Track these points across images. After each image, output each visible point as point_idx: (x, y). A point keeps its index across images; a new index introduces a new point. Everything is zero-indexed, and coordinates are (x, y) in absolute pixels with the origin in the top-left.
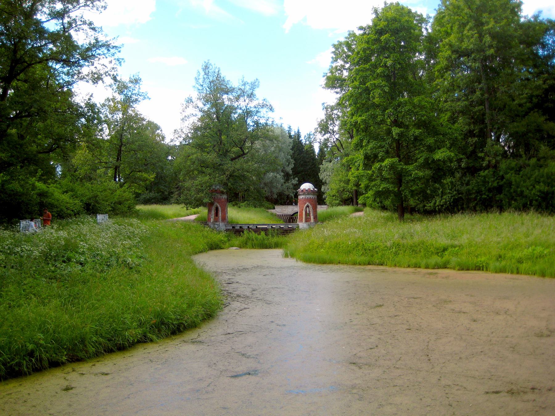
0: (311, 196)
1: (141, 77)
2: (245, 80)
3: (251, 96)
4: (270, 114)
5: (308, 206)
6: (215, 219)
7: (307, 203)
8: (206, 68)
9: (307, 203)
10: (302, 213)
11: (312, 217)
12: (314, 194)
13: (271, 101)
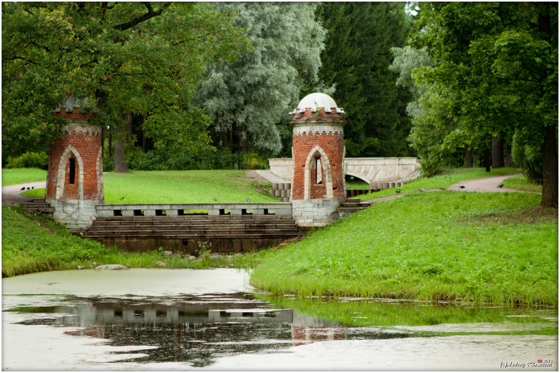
0: (328, 129)
5: (317, 157)
9: (317, 148)
12: (334, 123)
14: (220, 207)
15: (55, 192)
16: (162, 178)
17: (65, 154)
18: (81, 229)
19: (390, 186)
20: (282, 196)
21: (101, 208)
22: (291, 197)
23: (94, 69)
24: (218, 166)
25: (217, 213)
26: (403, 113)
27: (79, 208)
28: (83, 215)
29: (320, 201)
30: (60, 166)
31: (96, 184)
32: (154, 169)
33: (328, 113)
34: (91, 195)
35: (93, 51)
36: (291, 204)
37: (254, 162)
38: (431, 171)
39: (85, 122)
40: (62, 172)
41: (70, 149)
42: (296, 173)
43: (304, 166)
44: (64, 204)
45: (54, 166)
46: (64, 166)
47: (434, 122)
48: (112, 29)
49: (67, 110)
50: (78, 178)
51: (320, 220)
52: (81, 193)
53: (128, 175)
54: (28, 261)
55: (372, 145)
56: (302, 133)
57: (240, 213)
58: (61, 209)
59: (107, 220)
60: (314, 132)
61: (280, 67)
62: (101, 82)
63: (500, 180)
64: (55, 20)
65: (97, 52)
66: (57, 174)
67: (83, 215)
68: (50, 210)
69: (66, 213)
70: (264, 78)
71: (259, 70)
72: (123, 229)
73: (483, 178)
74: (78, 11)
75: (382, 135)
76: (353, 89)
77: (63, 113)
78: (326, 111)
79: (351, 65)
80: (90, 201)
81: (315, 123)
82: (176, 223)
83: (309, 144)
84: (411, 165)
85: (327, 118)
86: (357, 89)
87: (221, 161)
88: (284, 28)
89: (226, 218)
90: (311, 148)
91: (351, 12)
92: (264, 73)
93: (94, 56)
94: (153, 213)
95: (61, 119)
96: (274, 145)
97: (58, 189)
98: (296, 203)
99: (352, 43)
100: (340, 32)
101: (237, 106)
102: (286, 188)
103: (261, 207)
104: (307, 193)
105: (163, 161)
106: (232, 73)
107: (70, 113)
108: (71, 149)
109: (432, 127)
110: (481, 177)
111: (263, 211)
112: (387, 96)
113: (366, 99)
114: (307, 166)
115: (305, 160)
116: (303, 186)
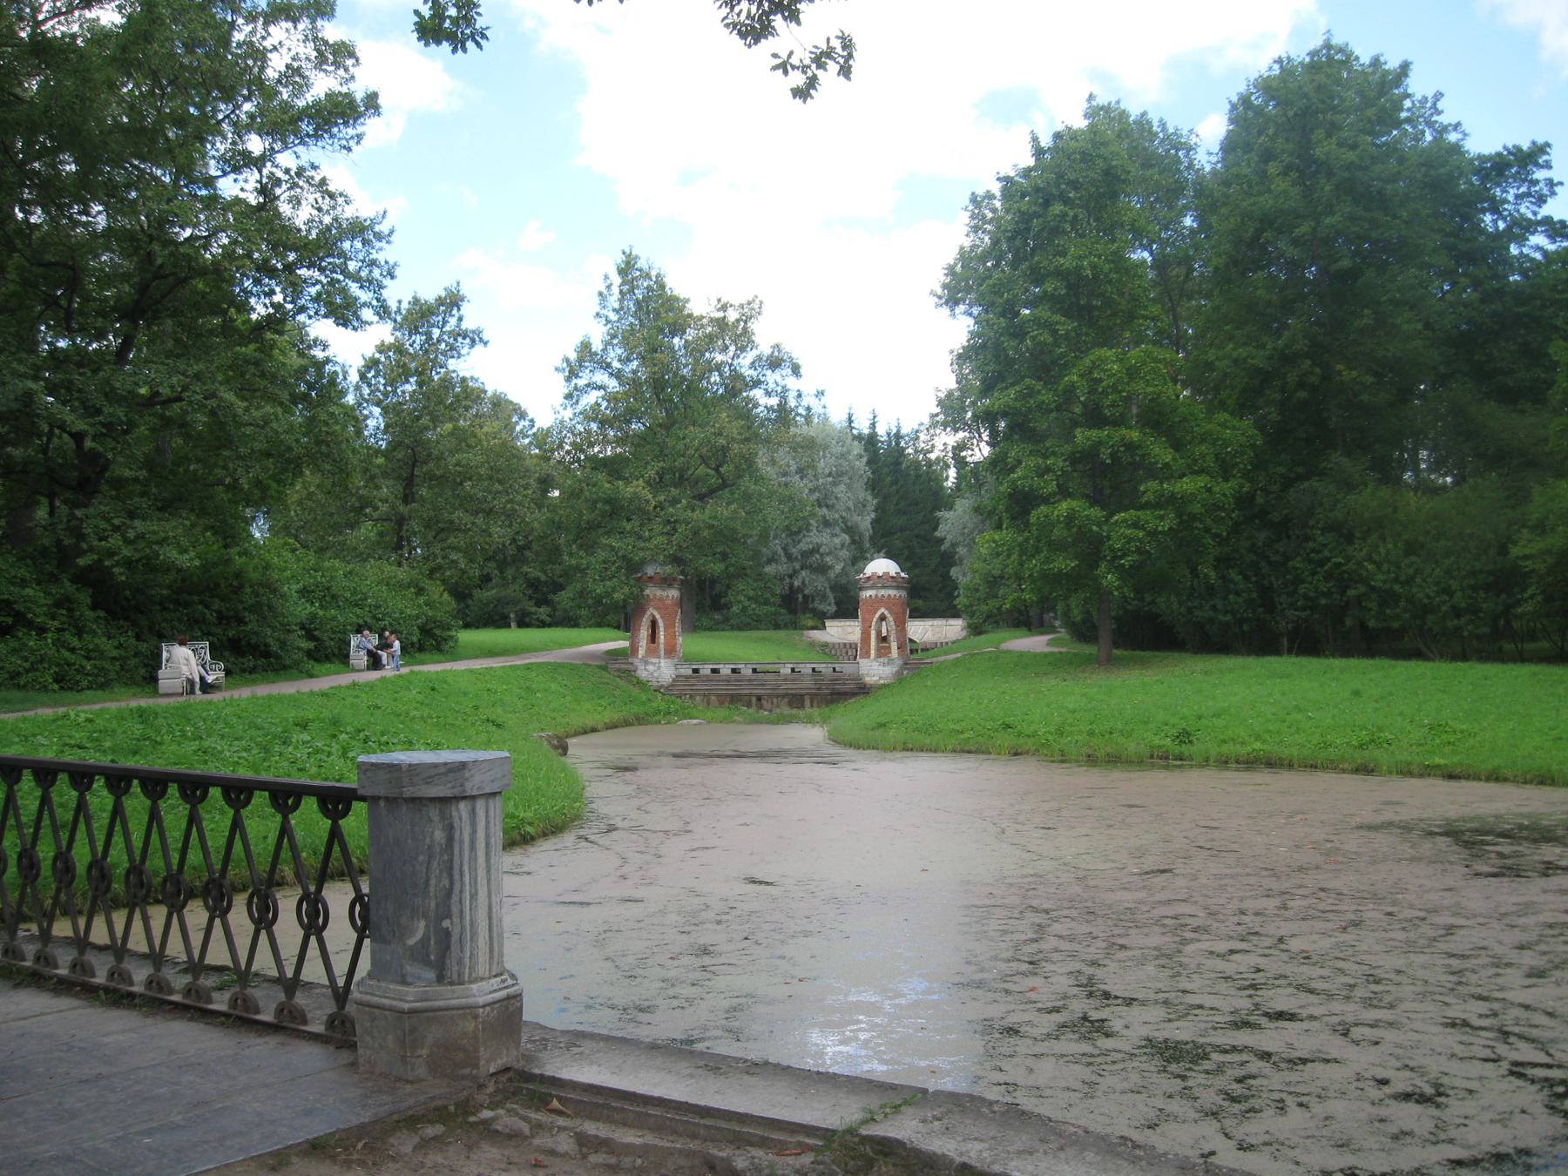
0: (892, 592)
1: (372, 89)
2: (724, 301)
3: (743, 340)
4: (792, 383)
5: (883, 618)
8: (628, 268)
11: (894, 645)
12: (897, 588)
13: (793, 349)
16: (763, 639)
24: (777, 627)
26: (946, 577)
37: (810, 623)
38: (975, 630)
40: (644, 633)
44: (646, 663)
54: (616, 716)
63: (1046, 638)
70: (819, 546)
71: (814, 538)
84: (953, 628)
95: (642, 581)
98: (863, 662)
109: (977, 590)
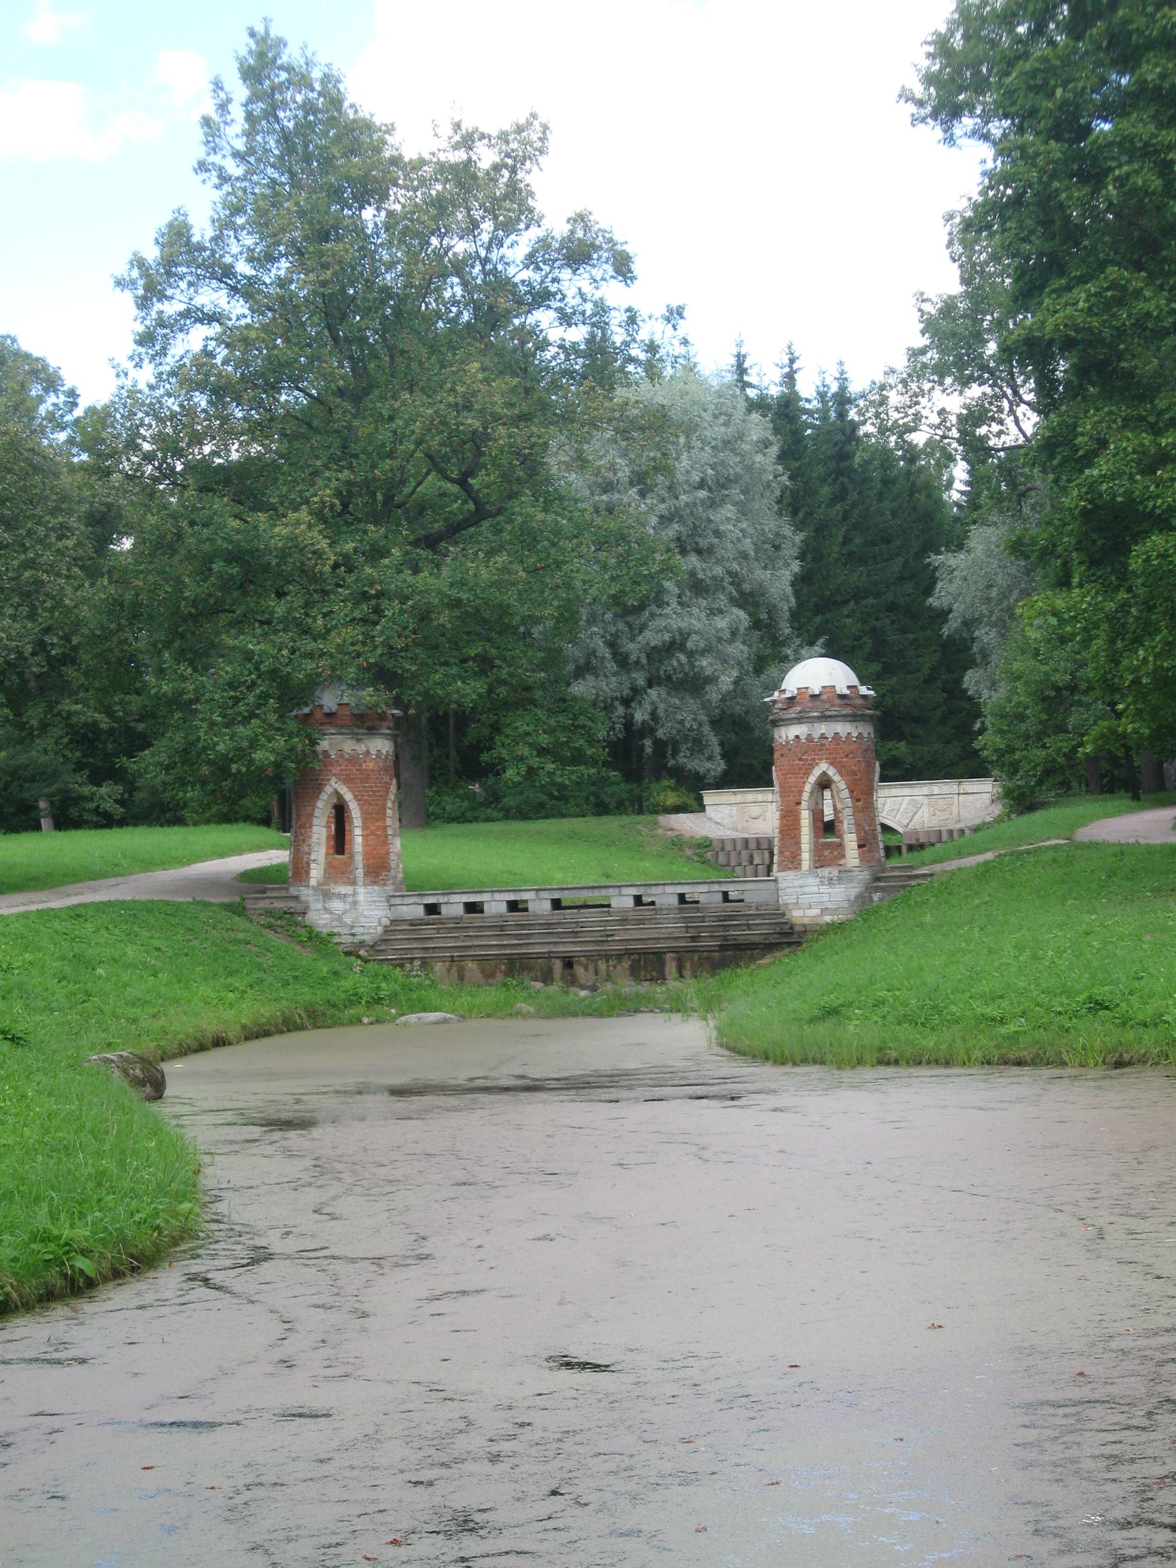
0: (842, 728)
2: (467, 126)
3: (512, 207)
4: (615, 294)
5: (824, 784)
6: (330, 866)
7: (823, 767)
8: (261, 65)
9: (823, 767)
10: (797, 820)
11: (851, 841)
12: (854, 718)
13: (615, 221)
14: (634, 891)
15: (308, 873)
16: (573, 837)
17: (324, 796)
18: (362, 944)
19: (956, 835)
20: (733, 863)
21: (398, 901)
22: (775, 866)
23: (378, 627)
24: (602, 809)
25: (630, 903)
26: (955, 692)
27: (355, 903)
28: (365, 917)
29: (834, 872)
30: (315, 821)
31: (388, 853)
32: (476, 819)
33: (842, 697)
34: (377, 875)
35: (373, 592)
36: (776, 880)
37: (671, 799)
38: (1022, 802)
39: (361, 731)
40: (320, 832)
41: (335, 786)
42: (782, 817)
43: (799, 804)
44: (327, 896)
45: (303, 820)
46: (324, 820)
47: (1026, 708)
48: (409, 548)
49: (326, 710)
50: (351, 842)
51: (835, 911)
52: (360, 872)
53: (430, 833)
54: (268, 1011)
55: (894, 756)
56: (791, 737)
57: (674, 901)
58: (320, 906)
59: (412, 923)
60: (816, 736)
61: (714, 612)
62: (391, 652)
64: (292, 532)
65: (380, 595)
66: (310, 837)
67: (365, 917)
68: (299, 908)
69: (331, 913)
72: (492, 944)
73: (1127, 812)
74: (340, 515)
75: (913, 736)
76: (853, 648)
77: (318, 715)
78: (838, 692)
79: (848, 601)
80: (376, 888)
81: (818, 717)
82: (548, 925)
83: (807, 760)
85: (840, 706)
86: (861, 647)
87: (606, 799)
88: (717, 533)
89: (647, 913)
90: (812, 767)
91: (843, 499)
92: (683, 625)
93: (374, 602)
94: (503, 908)
96: (709, 765)
97: (313, 865)
99: (852, 559)
100: (824, 537)
101: (634, 689)
102: (739, 848)
103: (716, 887)
104: (806, 857)
105: (492, 803)
106: (621, 625)
107: (330, 715)
108: (336, 786)
110: (1129, 811)
111: (720, 897)
112: (920, 660)
113: (881, 665)
114: (804, 804)
115: (801, 792)
116: (798, 843)
